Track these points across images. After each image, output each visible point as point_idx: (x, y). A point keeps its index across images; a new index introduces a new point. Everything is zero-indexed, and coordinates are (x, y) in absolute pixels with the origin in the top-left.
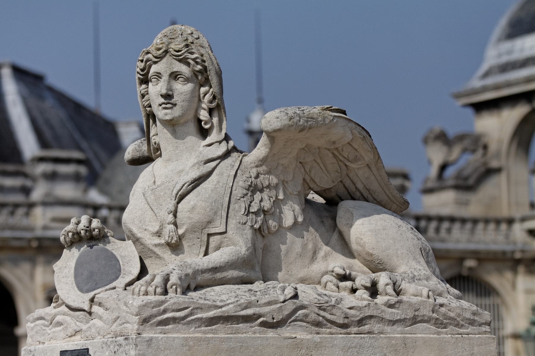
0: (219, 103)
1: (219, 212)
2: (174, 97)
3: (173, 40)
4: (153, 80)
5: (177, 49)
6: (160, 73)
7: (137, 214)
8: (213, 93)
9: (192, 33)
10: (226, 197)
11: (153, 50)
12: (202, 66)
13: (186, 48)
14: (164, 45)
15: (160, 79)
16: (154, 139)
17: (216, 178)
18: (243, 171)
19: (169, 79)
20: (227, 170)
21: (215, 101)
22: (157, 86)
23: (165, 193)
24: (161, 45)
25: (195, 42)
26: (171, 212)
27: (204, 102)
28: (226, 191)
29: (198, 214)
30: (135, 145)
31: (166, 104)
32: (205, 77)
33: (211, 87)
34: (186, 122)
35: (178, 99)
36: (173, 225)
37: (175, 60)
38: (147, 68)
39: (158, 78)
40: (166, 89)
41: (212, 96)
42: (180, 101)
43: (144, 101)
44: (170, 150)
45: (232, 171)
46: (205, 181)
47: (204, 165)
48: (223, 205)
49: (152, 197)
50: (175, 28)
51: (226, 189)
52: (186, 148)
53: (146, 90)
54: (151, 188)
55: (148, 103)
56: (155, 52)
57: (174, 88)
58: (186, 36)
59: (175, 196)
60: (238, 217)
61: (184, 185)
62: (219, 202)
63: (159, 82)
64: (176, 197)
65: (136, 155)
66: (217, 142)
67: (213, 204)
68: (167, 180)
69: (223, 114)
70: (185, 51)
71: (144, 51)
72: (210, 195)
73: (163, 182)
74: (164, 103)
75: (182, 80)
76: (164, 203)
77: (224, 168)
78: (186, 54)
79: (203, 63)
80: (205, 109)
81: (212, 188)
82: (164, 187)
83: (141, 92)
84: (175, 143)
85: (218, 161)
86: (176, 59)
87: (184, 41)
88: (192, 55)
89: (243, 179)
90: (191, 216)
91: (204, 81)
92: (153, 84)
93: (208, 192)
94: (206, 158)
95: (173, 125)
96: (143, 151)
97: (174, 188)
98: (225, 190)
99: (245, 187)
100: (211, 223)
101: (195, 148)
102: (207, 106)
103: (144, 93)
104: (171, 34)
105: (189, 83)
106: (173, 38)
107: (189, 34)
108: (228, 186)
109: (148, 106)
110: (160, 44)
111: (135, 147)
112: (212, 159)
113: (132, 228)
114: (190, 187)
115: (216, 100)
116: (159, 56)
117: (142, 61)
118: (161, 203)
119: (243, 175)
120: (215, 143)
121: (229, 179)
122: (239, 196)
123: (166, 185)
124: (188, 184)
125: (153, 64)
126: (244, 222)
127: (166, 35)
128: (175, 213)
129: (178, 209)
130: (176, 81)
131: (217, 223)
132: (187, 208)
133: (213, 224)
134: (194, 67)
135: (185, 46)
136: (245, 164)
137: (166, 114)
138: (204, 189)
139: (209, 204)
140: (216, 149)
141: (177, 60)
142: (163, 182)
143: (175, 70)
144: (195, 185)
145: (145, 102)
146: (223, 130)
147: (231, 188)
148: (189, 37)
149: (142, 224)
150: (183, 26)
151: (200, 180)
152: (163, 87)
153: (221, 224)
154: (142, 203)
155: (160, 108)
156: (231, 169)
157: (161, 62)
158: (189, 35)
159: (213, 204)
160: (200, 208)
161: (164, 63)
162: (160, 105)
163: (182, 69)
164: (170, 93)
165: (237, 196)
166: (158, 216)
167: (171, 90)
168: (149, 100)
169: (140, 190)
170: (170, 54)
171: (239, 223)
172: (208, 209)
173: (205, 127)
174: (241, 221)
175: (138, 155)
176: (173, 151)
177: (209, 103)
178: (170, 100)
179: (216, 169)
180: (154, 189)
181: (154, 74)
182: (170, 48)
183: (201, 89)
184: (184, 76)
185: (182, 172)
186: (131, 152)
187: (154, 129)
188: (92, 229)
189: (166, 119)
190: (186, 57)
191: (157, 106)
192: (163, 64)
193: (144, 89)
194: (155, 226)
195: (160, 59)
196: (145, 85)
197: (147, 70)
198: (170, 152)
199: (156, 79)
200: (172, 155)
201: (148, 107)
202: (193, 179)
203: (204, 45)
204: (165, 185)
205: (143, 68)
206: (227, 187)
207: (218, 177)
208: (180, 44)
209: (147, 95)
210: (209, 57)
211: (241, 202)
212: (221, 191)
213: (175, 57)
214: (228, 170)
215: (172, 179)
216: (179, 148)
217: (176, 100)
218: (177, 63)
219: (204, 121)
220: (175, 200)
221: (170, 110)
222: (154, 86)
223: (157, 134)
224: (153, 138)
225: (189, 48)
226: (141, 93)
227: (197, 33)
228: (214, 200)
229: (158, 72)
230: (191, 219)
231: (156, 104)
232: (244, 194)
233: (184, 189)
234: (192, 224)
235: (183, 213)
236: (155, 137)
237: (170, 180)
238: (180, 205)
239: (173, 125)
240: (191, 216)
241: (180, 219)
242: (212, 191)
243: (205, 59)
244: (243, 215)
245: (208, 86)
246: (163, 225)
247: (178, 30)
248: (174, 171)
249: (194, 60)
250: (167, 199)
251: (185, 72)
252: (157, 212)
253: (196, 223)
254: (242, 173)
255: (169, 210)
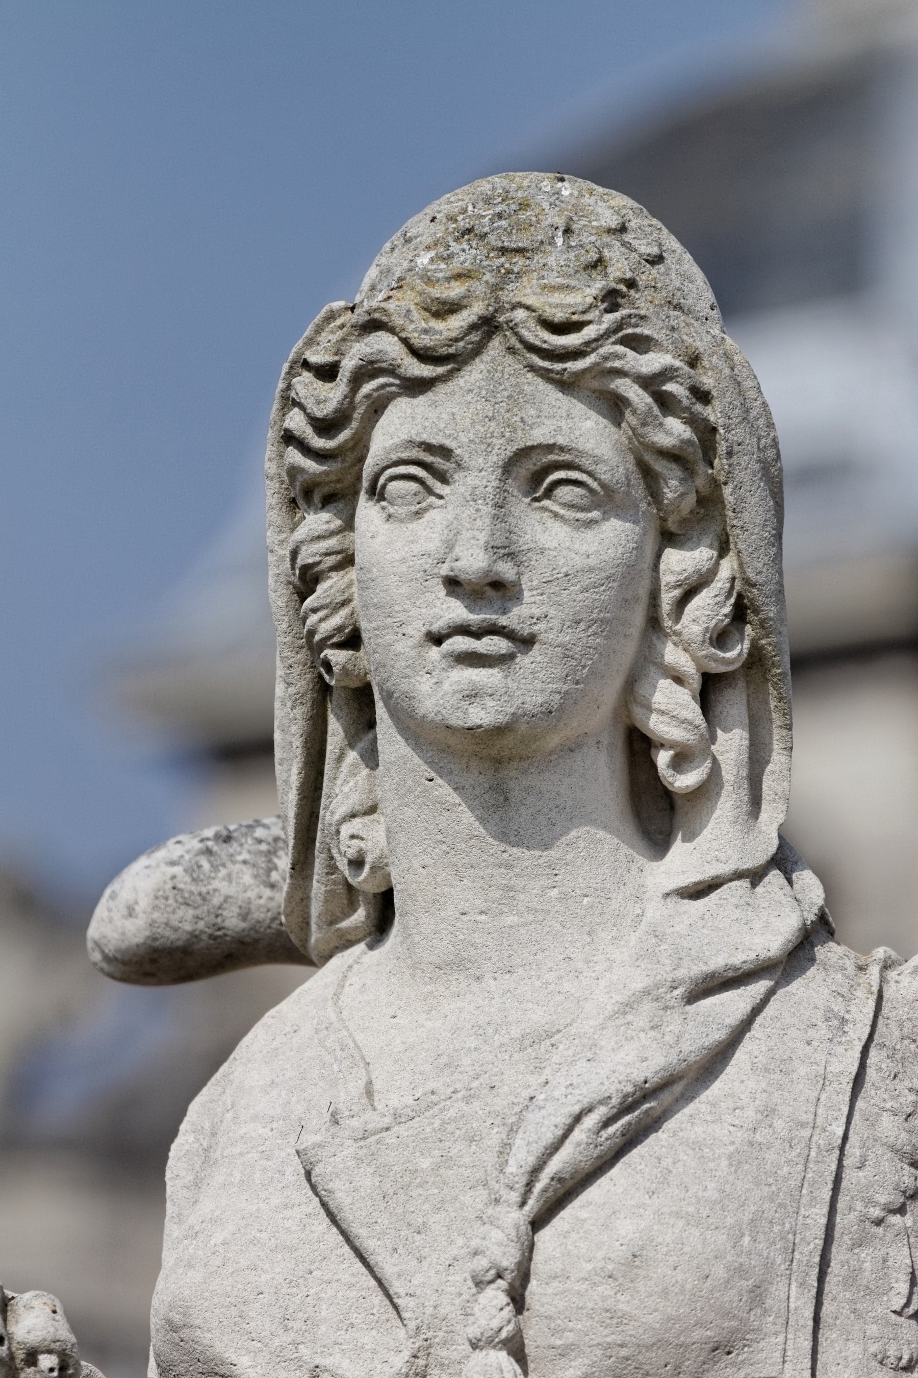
0: (762, 648)
1: (773, 1289)
2: (526, 594)
3: (519, 262)
4: (393, 486)
5: (559, 316)
6: (445, 452)
7: (264, 1277)
8: (738, 586)
9: (623, 229)
10: (813, 1202)
11: (409, 311)
12: (693, 421)
13: (608, 311)
14: (479, 288)
15: (438, 487)
16: (353, 837)
17: (751, 1084)
18: (898, 1057)
19: (502, 490)
20: (809, 1043)
21: (742, 633)
22: (415, 526)
23: (446, 1161)
24: (453, 283)
25: (642, 280)
26: (499, 1276)
27: (678, 634)
28: (811, 1165)
29: (665, 1293)
30: (173, 863)
31: (477, 633)
32: (701, 489)
33: (723, 549)
34: (572, 748)
35: (544, 609)
36: (504, 1354)
37: (539, 380)
38: (355, 416)
39: (431, 481)
40: (487, 542)
41: (732, 600)
42: (556, 623)
43: (314, 611)
44: (463, 906)
45: (840, 1050)
46: (692, 1098)
47: (688, 1008)
48: (793, 1251)
49: (366, 1180)
50: (520, 188)
51: (813, 1154)
52: (563, 898)
53: (332, 543)
54: (355, 1123)
55: (336, 620)
56: (424, 325)
57: (524, 541)
58: (593, 238)
59: (524, 1180)
60: (874, 1327)
61: (578, 1119)
62: (776, 1229)
63: (432, 499)
64: (529, 1186)
65: (175, 923)
66: (738, 875)
67: (747, 1239)
68: (458, 1086)
69: (774, 715)
70: (604, 326)
71: (331, 317)
72: (728, 1188)
73: (433, 1093)
74: (464, 630)
75: (577, 501)
76: (437, 1217)
77: (793, 1032)
78: (608, 348)
79: (698, 407)
80: (679, 680)
81: (733, 1143)
82: (437, 1123)
83: (294, 554)
84: (500, 866)
85: (761, 986)
86: (545, 375)
87: (586, 268)
88: (638, 356)
89: (902, 1100)
90: (624, 1303)
91: (691, 512)
92: (391, 510)
93: (711, 1165)
94: (695, 969)
95: (498, 762)
96: (216, 900)
97: (512, 1130)
98: (807, 1160)
99: (908, 1148)
100: (729, 1353)
101: (614, 904)
102: (694, 659)
103: (317, 559)
104: (503, 223)
105: (608, 520)
106: (519, 251)
107: (609, 231)
108: (819, 1140)
109: (335, 640)
110: (449, 279)
111: (173, 877)
112: (731, 974)
113: (231, 1355)
114: (611, 1130)
115: (748, 629)
116: (444, 351)
117: (327, 373)
118: (420, 1220)
119: (895, 1076)
120: (731, 880)
121: (823, 1097)
122: (883, 1199)
123: (452, 1113)
124: (602, 1112)
125: (399, 395)
126: (906, 1357)
127: (469, 231)
128: (517, 1284)
129: (537, 1257)
130: (537, 504)
131: (764, 1355)
132: (600, 1255)
133: (743, 1361)
134: (649, 429)
135: (603, 301)
136: (903, 1012)
137: (473, 695)
138: (691, 1152)
139: (721, 1239)
140: (738, 913)
141: (550, 380)
142: (433, 1093)
143: (540, 435)
144: (639, 1120)
145: (321, 614)
146: (763, 807)
147: (837, 1153)
148: (608, 246)
149: (291, 1336)
150: (566, 184)
151: (666, 1097)
152: (466, 535)
153: (784, 1362)
154: (287, 1213)
155: (435, 652)
156: (830, 1040)
157: (451, 385)
158: (607, 239)
159: (747, 1239)
160: (672, 1260)
161: (471, 391)
162: (437, 639)
163: (577, 433)
164: (506, 570)
165: (869, 1202)
166: (402, 1291)
167: (511, 556)
168: (345, 603)
169: (261, 1131)
170: (513, 341)
171: (881, 1363)
172: (719, 1271)
173: (677, 784)
174: (892, 1352)
175: (188, 927)
176: (482, 912)
177: (711, 644)
178: (504, 613)
179: (748, 1035)
180: (375, 1134)
181: (405, 455)
182: (514, 307)
183: (664, 557)
184: (590, 474)
185: (548, 1042)
186: (144, 903)
187: (353, 774)
188: (20, 1355)
189: (469, 724)
190: (609, 365)
191: (411, 642)
192: (469, 398)
193: (320, 538)
194: (374, 1352)
195: (449, 367)
196: (325, 516)
197: (354, 424)
198: (464, 918)
199: (413, 486)
200: (477, 938)
201: (340, 646)
202: (630, 1089)
203: (690, 302)
204: (441, 1111)
205: (336, 411)
206: (819, 1147)
207: (763, 1085)
208: (573, 283)
209: (333, 574)
210: (727, 371)
211: (889, 1236)
212: (785, 1169)
213: (543, 358)
214: (815, 1043)
215: (485, 1079)
216: (522, 897)
217: (537, 612)
218: (552, 395)
219: (672, 745)
220: (523, 1204)
221: (495, 671)
222: (401, 521)
223: (372, 810)
224: (346, 829)
225: (624, 312)
226: (300, 562)
227: (648, 230)
228: (746, 1219)
229: (434, 442)
230: (618, 1324)
231: (409, 630)
232: (904, 1192)
233: (578, 1144)
234: (624, 1352)
235: (568, 1285)
236: (357, 821)
237: (475, 1084)
238: (545, 1236)
239: (498, 762)
240: (621, 1306)
241: (549, 1318)
242: (736, 1161)
243: (707, 381)
244: (899, 1313)
245: (707, 540)
246: (430, 1346)
247: (546, 205)
248: (490, 1031)
249: (650, 383)
250: (456, 1198)
251: (597, 452)
252: (396, 1269)
253: (649, 1348)
254: (894, 1067)
255: (482, 1263)
